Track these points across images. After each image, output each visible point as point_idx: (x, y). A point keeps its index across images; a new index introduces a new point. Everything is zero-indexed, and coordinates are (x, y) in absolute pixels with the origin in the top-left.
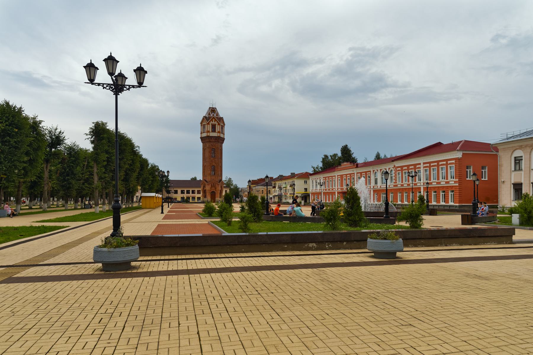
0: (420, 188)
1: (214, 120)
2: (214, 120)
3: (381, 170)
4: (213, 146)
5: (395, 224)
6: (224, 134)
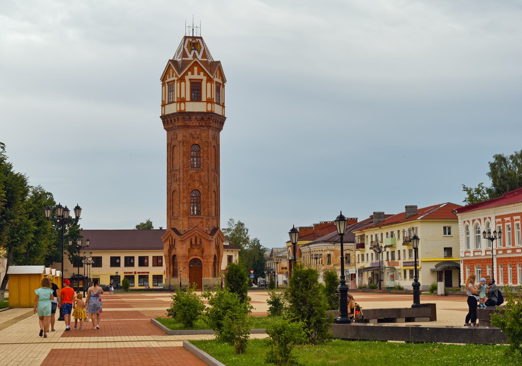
1: (196, 69)
2: (196, 69)
4: (193, 138)
6: (223, 106)
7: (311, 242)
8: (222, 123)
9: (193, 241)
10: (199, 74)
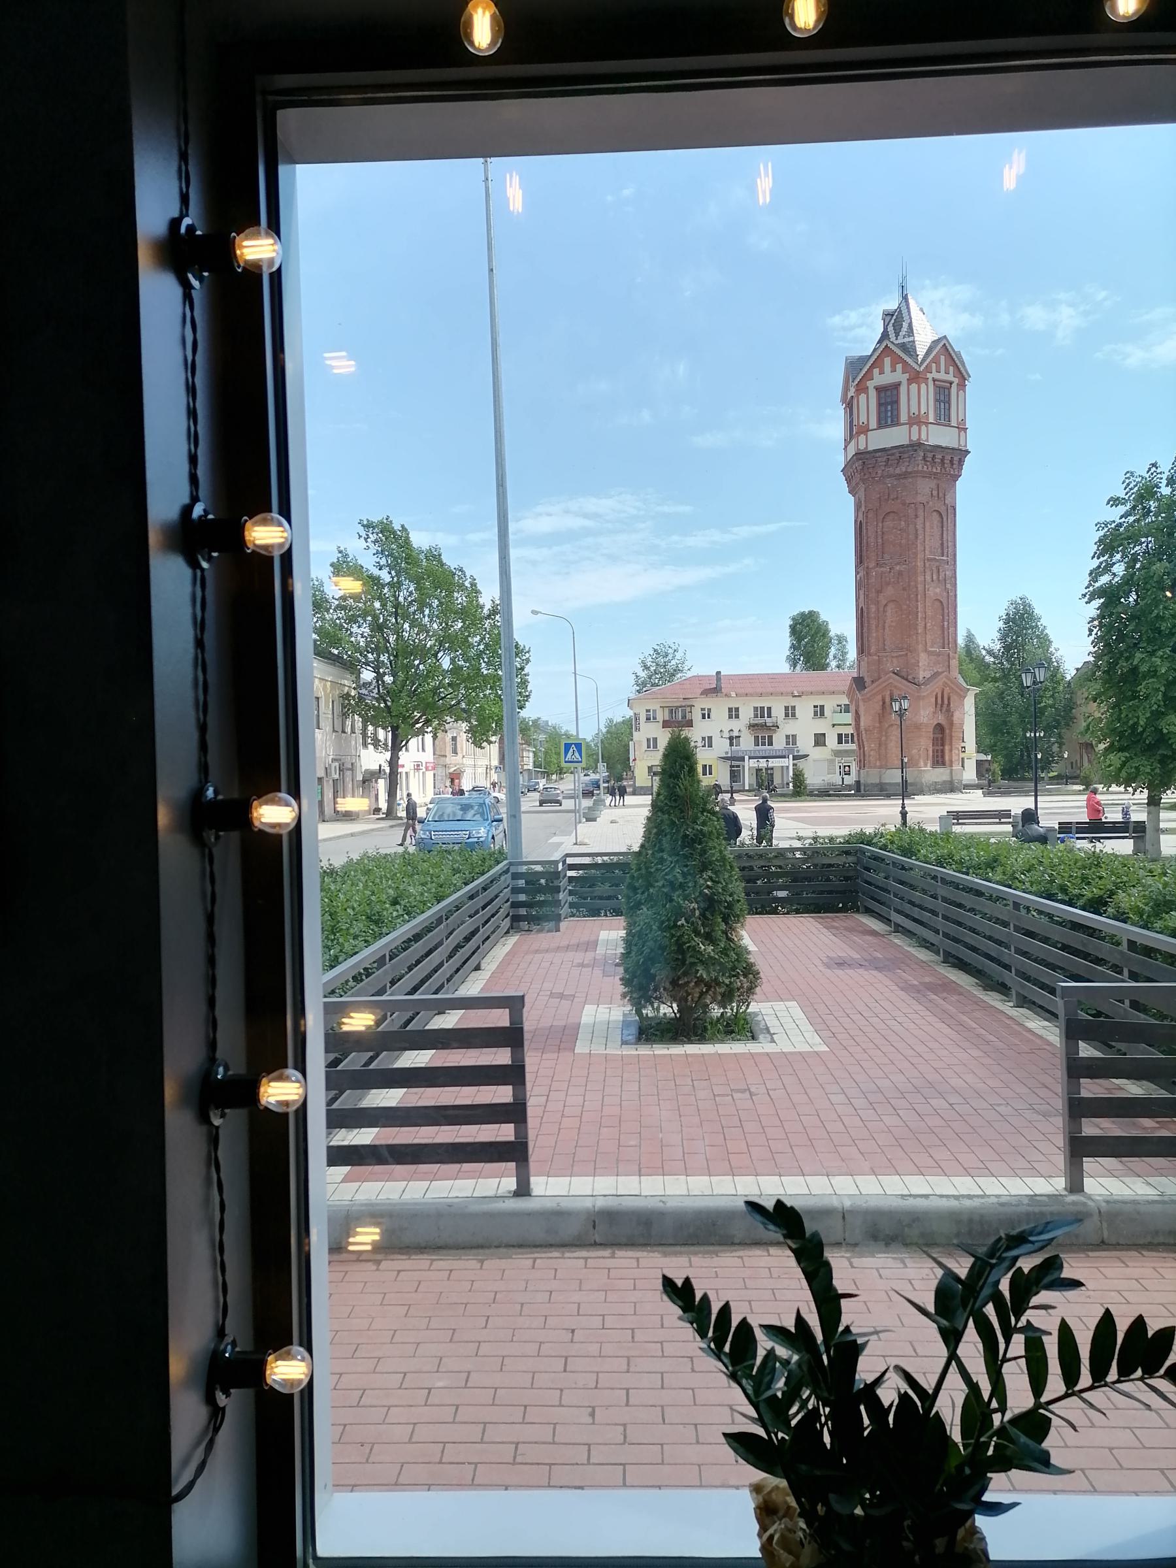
1: (887, 361)
2: (887, 361)
10: (894, 370)
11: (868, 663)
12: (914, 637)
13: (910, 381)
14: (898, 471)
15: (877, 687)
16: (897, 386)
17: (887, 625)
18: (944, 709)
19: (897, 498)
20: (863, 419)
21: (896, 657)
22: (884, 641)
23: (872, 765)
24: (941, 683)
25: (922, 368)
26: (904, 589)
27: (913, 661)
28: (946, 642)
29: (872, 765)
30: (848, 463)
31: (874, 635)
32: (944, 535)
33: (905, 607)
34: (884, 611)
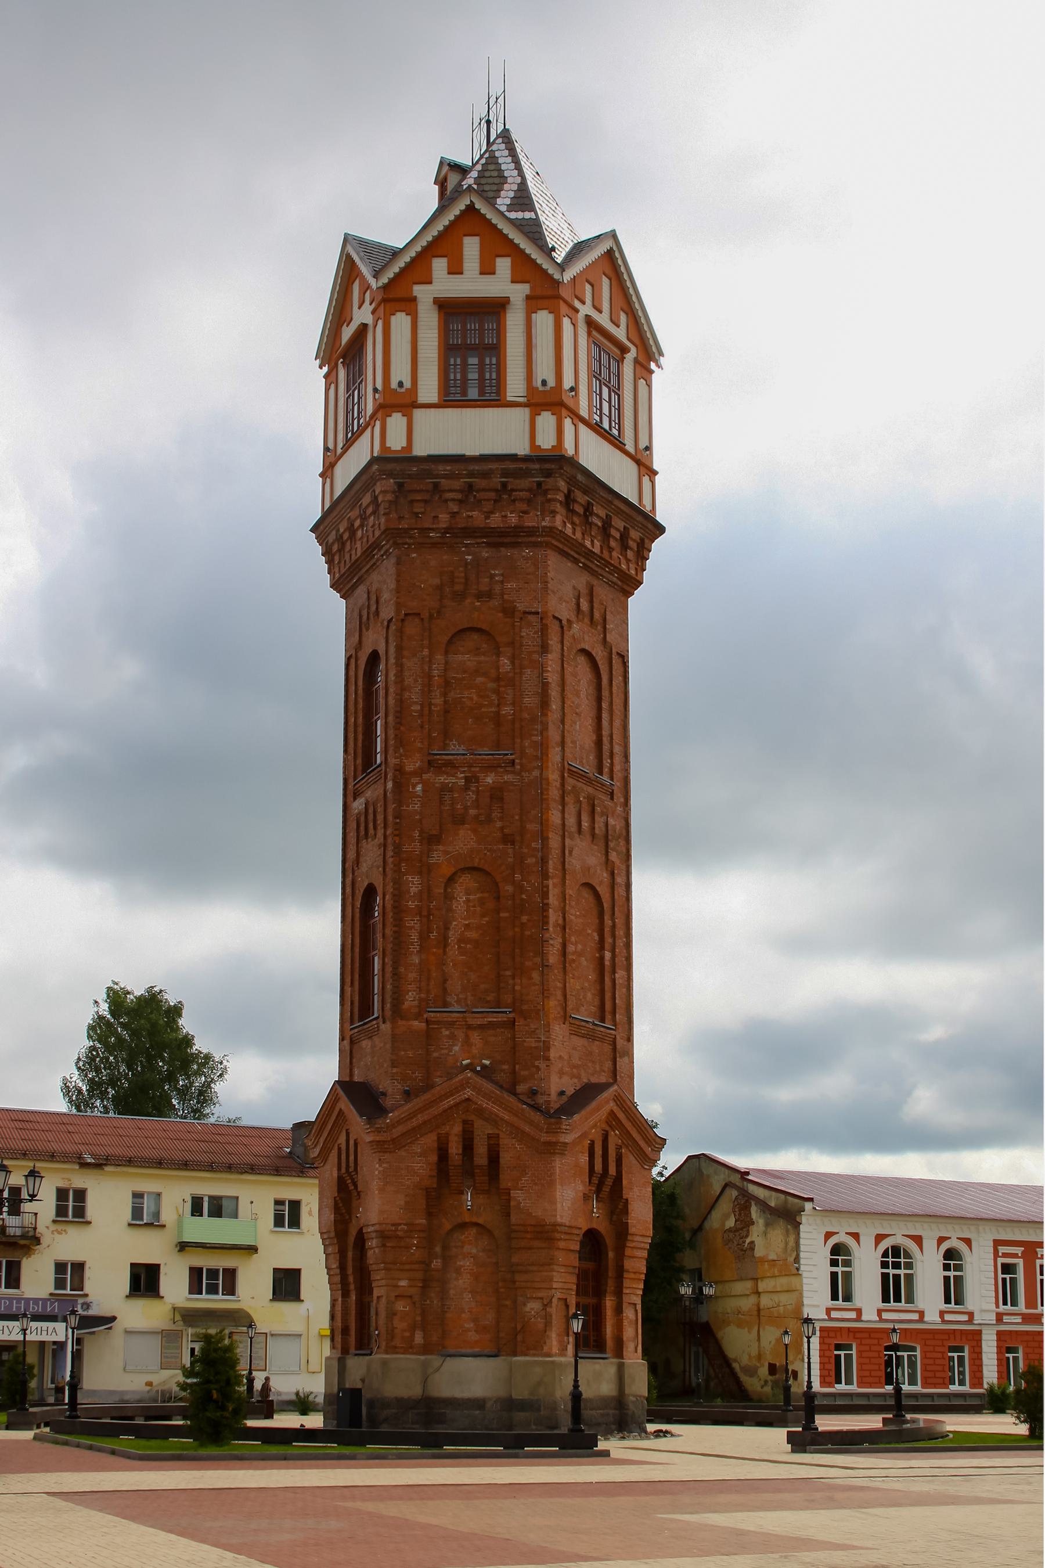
0: (975, 1337)
1: (471, 247)
2: (471, 247)
3: (879, 1238)
5: (597, 1447)
7: (370, 1507)
8: (1042, 1190)
9: (455, 1149)
10: (487, 269)
11: (394, 1037)
12: (536, 976)
13: (533, 303)
14: (495, 520)
15: (421, 1110)
16: (497, 307)
17: (453, 936)
18: (606, 1189)
19: (489, 595)
20: (401, 372)
21: (481, 1027)
22: (445, 981)
23: (397, 1342)
24: (603, 1114)
25: (567, 276)
26: (507, 839)
27: (531, 1042)
28: (608, 1006)
29: (397, 1342)
30: (335, 505)
31: (416, 960)
32: (605, 723)
33: (510, 888)
34: (448, 897)
